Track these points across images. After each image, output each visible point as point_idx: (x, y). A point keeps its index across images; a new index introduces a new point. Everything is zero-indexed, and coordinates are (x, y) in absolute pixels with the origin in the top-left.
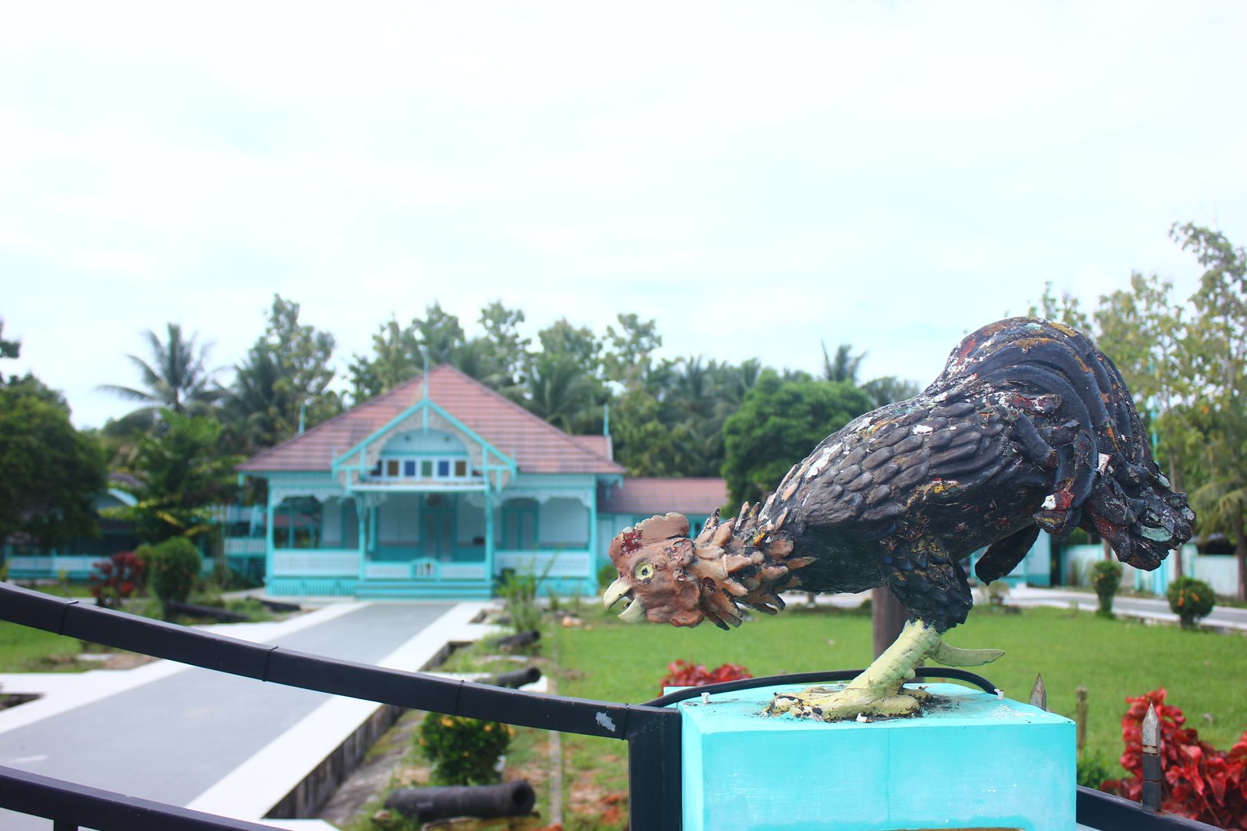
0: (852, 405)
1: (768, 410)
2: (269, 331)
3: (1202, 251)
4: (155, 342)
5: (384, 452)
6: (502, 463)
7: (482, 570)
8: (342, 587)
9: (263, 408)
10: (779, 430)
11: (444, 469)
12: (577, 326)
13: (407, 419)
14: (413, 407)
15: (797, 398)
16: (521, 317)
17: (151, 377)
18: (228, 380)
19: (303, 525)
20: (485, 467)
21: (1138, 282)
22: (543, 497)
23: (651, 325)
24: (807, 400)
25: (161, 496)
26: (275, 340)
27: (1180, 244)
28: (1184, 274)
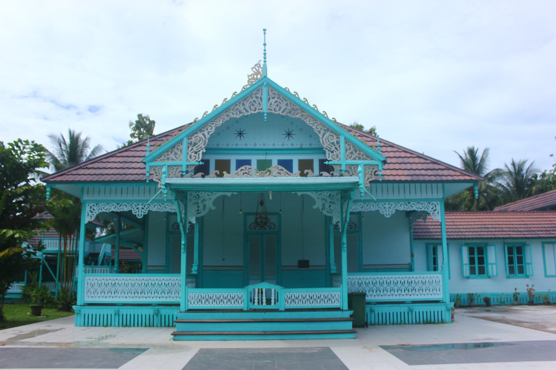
6: (368, 157)
7: (337, 296)
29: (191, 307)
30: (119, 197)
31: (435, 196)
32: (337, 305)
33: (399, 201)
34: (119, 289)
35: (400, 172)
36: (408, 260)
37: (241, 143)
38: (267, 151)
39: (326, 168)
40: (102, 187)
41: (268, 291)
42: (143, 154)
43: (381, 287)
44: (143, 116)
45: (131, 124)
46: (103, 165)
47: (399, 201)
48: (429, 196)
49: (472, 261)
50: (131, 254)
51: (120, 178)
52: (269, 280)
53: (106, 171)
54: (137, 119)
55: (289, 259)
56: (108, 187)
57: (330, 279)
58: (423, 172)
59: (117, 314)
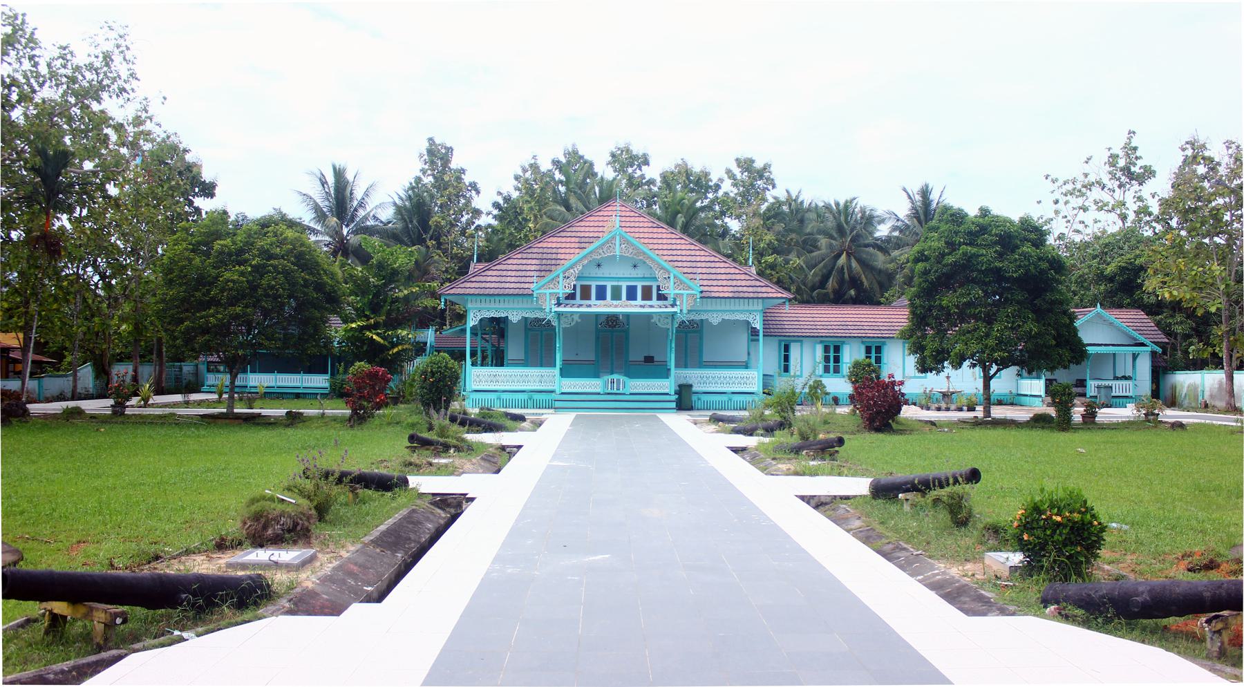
0: (1033, 236)
1: (958, 239)
2: (424, 172)
4: (324, 183)
5: (579, 278)
6: (690, 288)
7: (667, 386)
8: (556, 403)
9: (421, 241)
10: (970, 258)
11: (631, 294)
12: (697, 169)
13: (601, 246)
14: (607, 237)
15: (983, 229)
16: (646, 162)
18: (387, 214)
19: (495, 343)
20: (671, 291)
22: (715, 319)
23: (766, 168)
25: (368, 318)
26: (428, 180)
30: (497, 306)
31: (755, 308)
32: (666, 391)
35: (725, 289)
36: (745, 358)
37: (599, 273)
38: (619, 279)
39: (662, 297)
41: (618, 381)
43: (702, 379)
44: (437, 142)
45: (421, 156)
48: (751, 308)
49: (827, 359)
52: (620, 373)
55: (636, 355)
57: (666, 374)
58: (745, 289)
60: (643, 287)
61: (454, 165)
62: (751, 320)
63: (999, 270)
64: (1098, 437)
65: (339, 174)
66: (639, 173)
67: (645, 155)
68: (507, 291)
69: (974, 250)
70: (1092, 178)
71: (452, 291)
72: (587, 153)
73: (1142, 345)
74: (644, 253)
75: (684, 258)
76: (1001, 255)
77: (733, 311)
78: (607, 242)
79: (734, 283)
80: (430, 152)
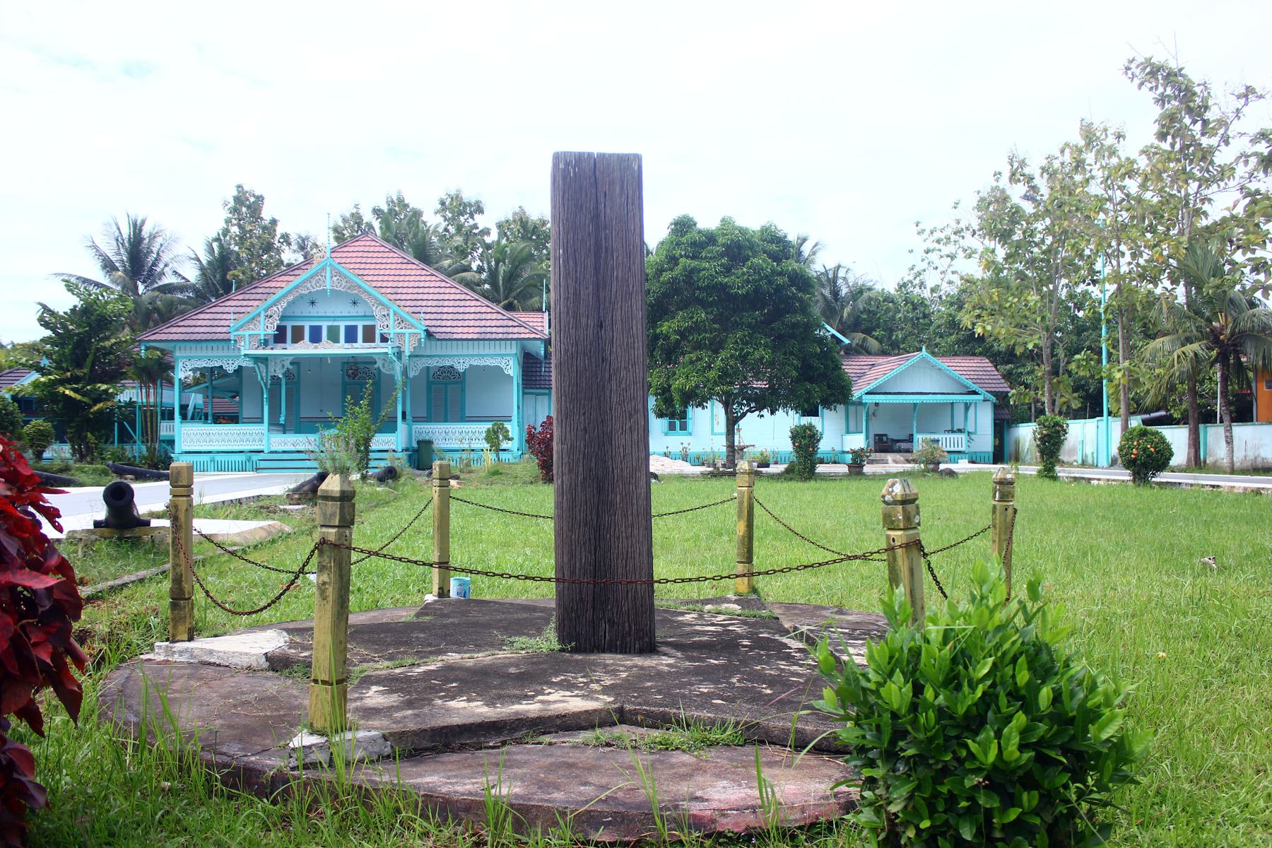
1: (677, 252)
3: (1161, 89)
6: (413, 326)
10: (691, 272)
17: (108, 266)
18: (192, 274)
20: (392, 331)
21: (1089, 136)
22: (461, 368)
24: (721, 240)
27: (1137, 81)
28: (1137, 124)
29: (273, 449)
30: (210, 353)
33: (473, 356)
34: (214, 438)
35: (471, 330)
37: (313, 311)
40: (193, 345)
42: (227, 323)
44: (246, 189)
46: (193, 323)
47: (473, 356)
50: (225, 404)
51: (210, 337)
53: (197, 330)
54: (235, 193)
56: (199, 345)
58: (494, 330)
59: (213, 460)
60: (365, 327)
61: (266, 215)
62: (503, 366)
63: (724, 287)
64: (864, 484)
65: (137, 228)
66: (471, 222)
67: (478, 202)
68: (216, 336)
69: (695, 263)
70: (962, 225)
71: (153, 338)
72: (413, 202)
73: (974, 393)
74: (360, 287)
75: (431, 297)
76: (728, 270)
77: (483, 356)
78: (316, 274)
79: (483, 323)
80: (238, 200)
